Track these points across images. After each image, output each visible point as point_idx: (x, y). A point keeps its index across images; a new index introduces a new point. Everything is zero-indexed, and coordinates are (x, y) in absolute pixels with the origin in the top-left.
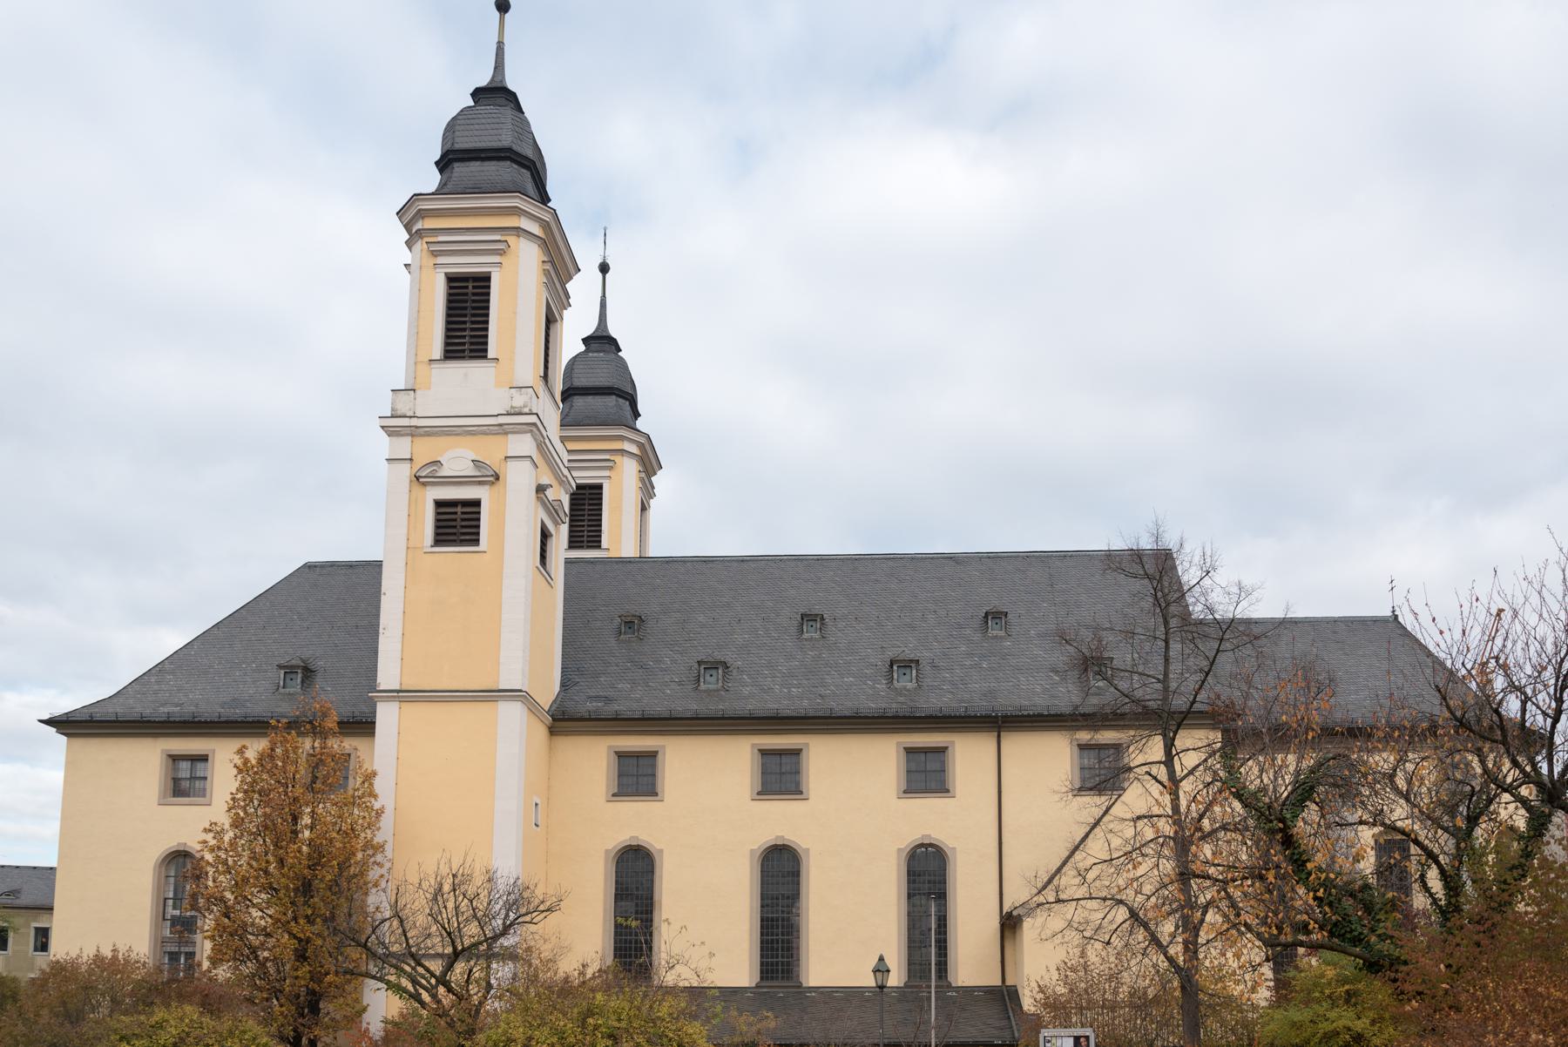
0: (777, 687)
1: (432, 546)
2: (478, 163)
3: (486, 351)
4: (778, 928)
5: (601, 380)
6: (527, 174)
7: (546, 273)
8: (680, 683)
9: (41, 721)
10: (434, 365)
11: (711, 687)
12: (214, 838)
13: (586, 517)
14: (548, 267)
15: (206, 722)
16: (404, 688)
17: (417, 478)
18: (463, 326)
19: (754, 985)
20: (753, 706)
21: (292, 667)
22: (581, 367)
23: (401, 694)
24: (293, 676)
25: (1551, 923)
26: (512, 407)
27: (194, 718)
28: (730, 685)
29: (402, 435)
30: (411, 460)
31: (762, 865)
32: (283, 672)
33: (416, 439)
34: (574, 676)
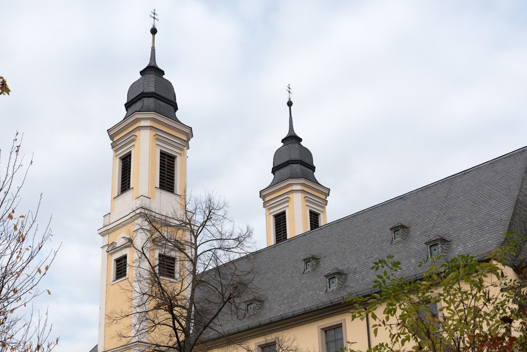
17: (108, 252)
25: (479, 318)
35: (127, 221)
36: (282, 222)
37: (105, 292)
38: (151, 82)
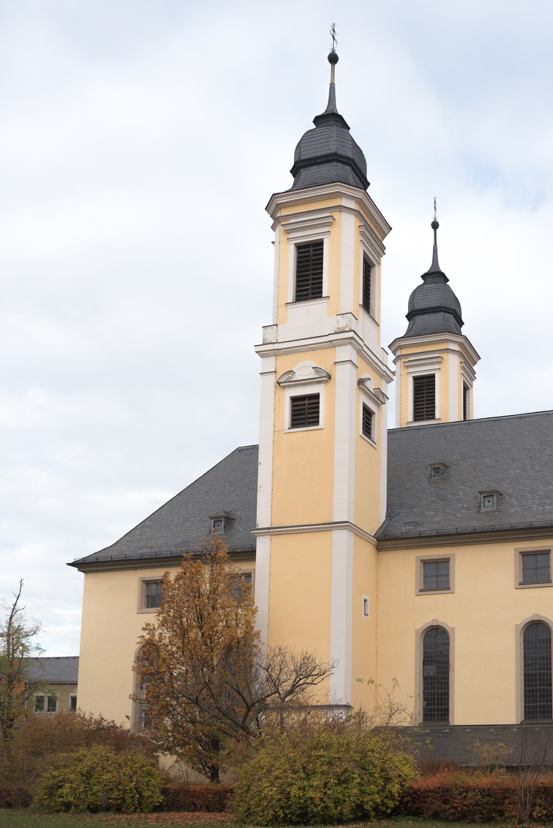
0: (535, 506)
1: (289, 429)
2: (316, 167)
3: (321, 292)
4: (536, 681)
5: (433, 302)
6: (348, 168)
7: (362, 234)
8: (468, 509)
9: (68, 564)
10: (289, 307)
11: (489, 509)
12: (148, 634)
13: (425, 398)
14: (463, 365)
15: (163, 558)
16: (274, 526)
17: (279, 383)
18: (308, 278)
19: (519, 723)
20: (516, 521)
21: (218, 517)
22: (420, 295)
23: (271, 530)
24: (219, 523)
26: (338, 328)
27: (142, 556)
28: (502, 507)
29: (270, 356)
30: (275, 372)
31: (525, 636)
32: (213, 521)
33: (278, 358)
34: (397, 509)
35: (322, 344)
36: (425, 388)
37: (272, 442)
38: (346, 140)
